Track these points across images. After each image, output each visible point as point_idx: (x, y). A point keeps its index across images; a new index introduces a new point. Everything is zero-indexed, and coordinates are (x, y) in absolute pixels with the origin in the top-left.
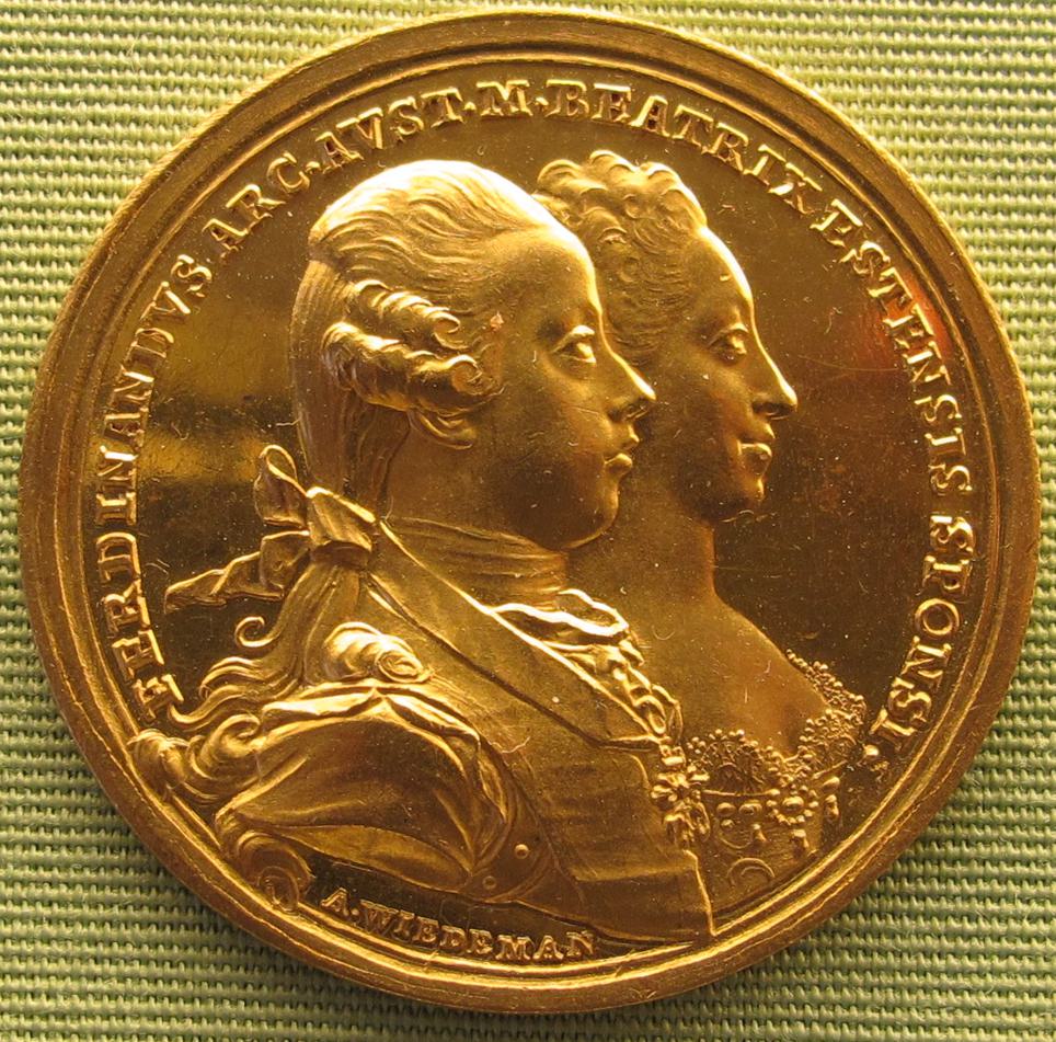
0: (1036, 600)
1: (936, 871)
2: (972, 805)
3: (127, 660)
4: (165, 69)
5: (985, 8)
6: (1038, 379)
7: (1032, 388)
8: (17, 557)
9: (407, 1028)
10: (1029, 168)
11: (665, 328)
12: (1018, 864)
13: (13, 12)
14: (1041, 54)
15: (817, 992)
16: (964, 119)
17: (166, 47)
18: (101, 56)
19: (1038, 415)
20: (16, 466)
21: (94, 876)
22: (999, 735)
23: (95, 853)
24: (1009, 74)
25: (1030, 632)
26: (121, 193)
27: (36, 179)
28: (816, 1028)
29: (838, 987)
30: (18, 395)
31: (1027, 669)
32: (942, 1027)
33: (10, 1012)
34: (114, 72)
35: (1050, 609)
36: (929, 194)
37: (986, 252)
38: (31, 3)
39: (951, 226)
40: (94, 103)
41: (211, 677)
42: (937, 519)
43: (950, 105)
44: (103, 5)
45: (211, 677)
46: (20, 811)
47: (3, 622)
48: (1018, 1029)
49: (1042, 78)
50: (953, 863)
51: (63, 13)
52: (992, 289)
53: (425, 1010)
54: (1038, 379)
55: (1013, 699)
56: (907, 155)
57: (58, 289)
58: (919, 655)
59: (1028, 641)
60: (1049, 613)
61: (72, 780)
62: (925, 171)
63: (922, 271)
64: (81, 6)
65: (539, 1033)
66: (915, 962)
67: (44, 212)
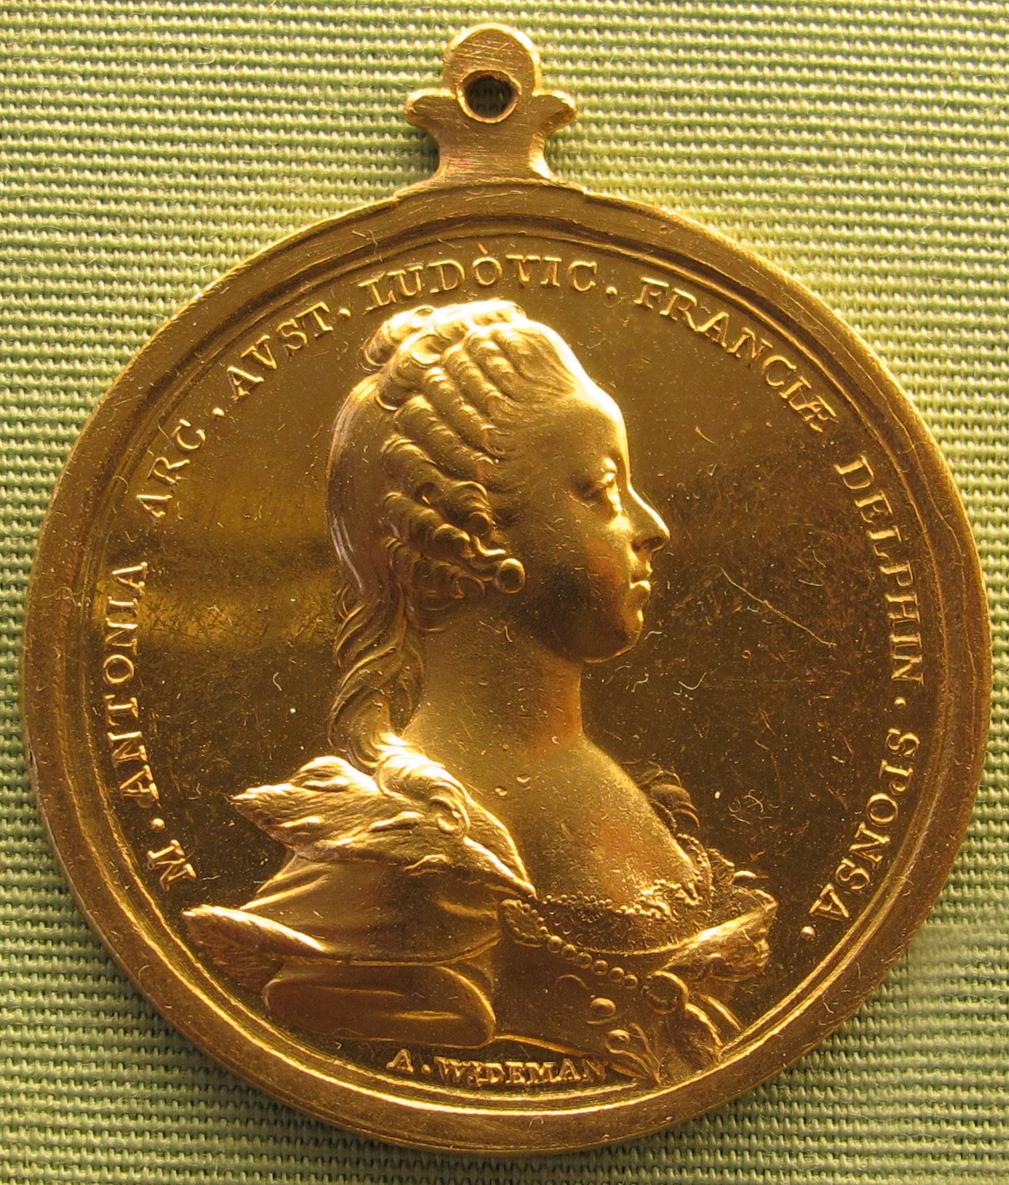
1: (830, 1112)
5: (222, 8)
7: (986, 570)
9: (354, 1160)
13: (10, 11)
16: (878, 338)
18: (218, 86)
25: (970, 829)
27: (733, 149)
29: (739, 1151)
31: (988, 776)
32: (831, 1172)
35: (1002, 606)
38: (15, 3)
41: (338, 702)
42: (893, 731)
44: (92, 5)
45: (338, 702)
48: (902, 1172)
49: (996, 69)
53: (372, 1145)
56: (860, 324)
57: (135, 345)
58: (865, 839)
59: (969, 837)
64: (59, 5)
65: (476, 1164)
67: (734, 162)
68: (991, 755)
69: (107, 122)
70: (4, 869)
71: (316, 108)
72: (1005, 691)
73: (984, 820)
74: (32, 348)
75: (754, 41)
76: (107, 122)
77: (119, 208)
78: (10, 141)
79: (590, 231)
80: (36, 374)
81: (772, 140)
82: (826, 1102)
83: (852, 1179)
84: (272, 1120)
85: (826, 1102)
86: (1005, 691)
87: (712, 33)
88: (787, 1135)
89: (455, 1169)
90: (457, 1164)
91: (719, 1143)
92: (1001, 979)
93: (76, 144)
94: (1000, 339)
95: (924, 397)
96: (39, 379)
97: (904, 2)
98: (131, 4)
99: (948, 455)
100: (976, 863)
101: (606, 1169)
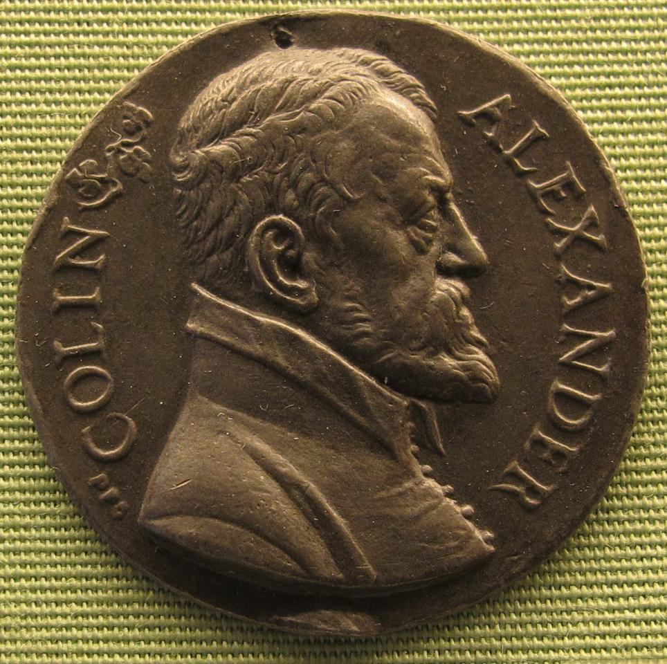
2: (601, 547)
7: (654, 298)
17: (585, 38)
21: (16, 433)
22: (560, 575)
23: (52, 506)
25: (640, 417)
28: (479, 655)
30: (11, 276)
34: (53, 106)
46: (116, 630)
50: (608, 535)
51: (55, 22)
55: (619, 524)
60: (661, 280)
61: (35, 458)
66: (587, 541)
69: (50, 56)
70: (3, 392)
74: (53, 38)
76: (50, 56)
77: (39, 108)
78: (8, 50)
80: (48, 80)
81: (551, 50)
84: (271, 640)
87: (13, 150)
88: (596, 559)
92: (662, 409)
93: (53, 16)
94: (608, 606)
95: (590, 114)
96: (102, 26)
97: (611, 1)
101: (501, 602)
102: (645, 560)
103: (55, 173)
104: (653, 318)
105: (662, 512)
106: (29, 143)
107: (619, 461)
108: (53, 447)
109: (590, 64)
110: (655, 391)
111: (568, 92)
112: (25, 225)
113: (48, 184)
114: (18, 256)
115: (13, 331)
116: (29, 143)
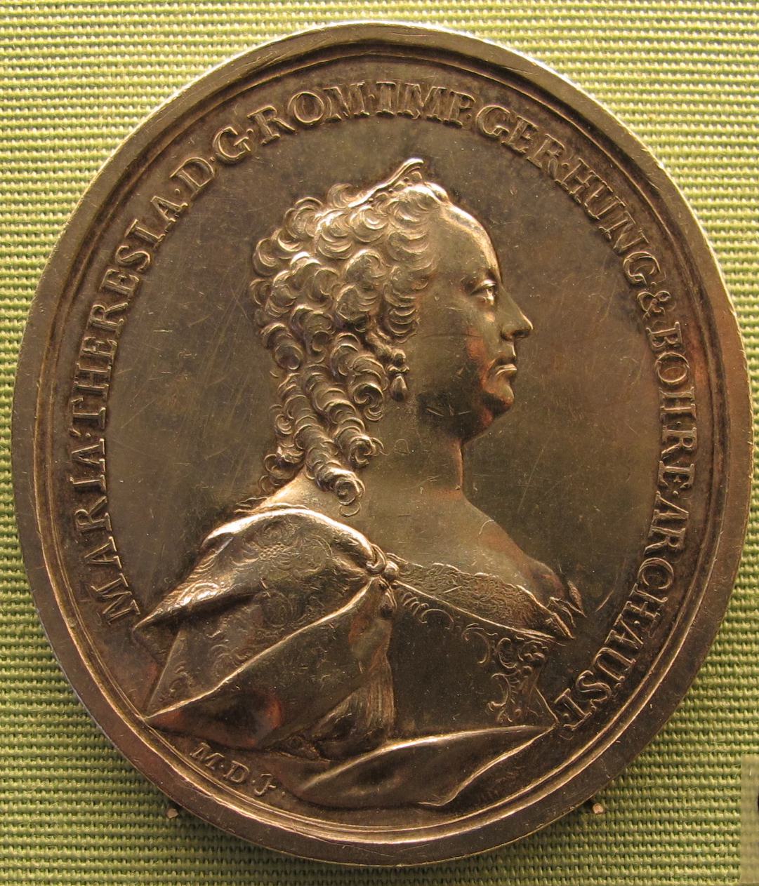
0: (748, 540)
3: (117, 557)
4: (184, 74)
6: (748, 330)
8: (10, 475)
10: (746, 49)
11: (394, 292)
12: (742, 744)
13: (7, 6)
14: (752, 283)
15: (604, 847)
19: (749, 350)
20: (11, 389)
24: (727, 55)
26: (122, 136)
32: (677, 878)
33: (4, 222)
36: (689, 200)
37: (701, 202)
39: (656, 156)
40: (739, 273)
43: (714, 198)
47: (1, 534)
52: (719, 256)
54: (748, 330)
62: (679, 176)
63: (264, 80)
68: (750, 534)
71: (542, 15)
72: (755, 712)
73: (713, 664)
75: (673, 45)
79: (639, 198)
82: (700, 742)
83: (692, 882)
85: (700, 742)
86: (755, 712)
89: (295, 863)
90: (277, 859)
91: (692, 704)
95: (682, 180)
98: (672, 3)
99: (732, 293)
100: (718, 760)
102: (742, 744)
103: (71, 212)
104: (749, 526)
105: (755, 149)
106: (25, 238)
107: (711, 645)
108: (119, 221)
109: (642, 40)
110: (748, 569)
111: (659, 150)
112: (30, 291)
113: (58, 232)
114: (22, 318)
115: (17, 537)
116: (25, 238)
